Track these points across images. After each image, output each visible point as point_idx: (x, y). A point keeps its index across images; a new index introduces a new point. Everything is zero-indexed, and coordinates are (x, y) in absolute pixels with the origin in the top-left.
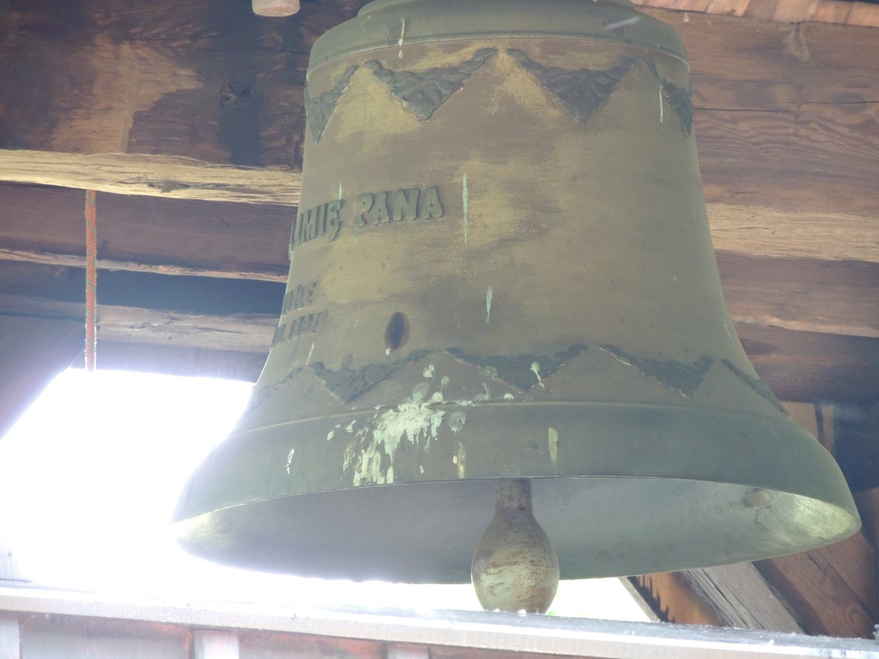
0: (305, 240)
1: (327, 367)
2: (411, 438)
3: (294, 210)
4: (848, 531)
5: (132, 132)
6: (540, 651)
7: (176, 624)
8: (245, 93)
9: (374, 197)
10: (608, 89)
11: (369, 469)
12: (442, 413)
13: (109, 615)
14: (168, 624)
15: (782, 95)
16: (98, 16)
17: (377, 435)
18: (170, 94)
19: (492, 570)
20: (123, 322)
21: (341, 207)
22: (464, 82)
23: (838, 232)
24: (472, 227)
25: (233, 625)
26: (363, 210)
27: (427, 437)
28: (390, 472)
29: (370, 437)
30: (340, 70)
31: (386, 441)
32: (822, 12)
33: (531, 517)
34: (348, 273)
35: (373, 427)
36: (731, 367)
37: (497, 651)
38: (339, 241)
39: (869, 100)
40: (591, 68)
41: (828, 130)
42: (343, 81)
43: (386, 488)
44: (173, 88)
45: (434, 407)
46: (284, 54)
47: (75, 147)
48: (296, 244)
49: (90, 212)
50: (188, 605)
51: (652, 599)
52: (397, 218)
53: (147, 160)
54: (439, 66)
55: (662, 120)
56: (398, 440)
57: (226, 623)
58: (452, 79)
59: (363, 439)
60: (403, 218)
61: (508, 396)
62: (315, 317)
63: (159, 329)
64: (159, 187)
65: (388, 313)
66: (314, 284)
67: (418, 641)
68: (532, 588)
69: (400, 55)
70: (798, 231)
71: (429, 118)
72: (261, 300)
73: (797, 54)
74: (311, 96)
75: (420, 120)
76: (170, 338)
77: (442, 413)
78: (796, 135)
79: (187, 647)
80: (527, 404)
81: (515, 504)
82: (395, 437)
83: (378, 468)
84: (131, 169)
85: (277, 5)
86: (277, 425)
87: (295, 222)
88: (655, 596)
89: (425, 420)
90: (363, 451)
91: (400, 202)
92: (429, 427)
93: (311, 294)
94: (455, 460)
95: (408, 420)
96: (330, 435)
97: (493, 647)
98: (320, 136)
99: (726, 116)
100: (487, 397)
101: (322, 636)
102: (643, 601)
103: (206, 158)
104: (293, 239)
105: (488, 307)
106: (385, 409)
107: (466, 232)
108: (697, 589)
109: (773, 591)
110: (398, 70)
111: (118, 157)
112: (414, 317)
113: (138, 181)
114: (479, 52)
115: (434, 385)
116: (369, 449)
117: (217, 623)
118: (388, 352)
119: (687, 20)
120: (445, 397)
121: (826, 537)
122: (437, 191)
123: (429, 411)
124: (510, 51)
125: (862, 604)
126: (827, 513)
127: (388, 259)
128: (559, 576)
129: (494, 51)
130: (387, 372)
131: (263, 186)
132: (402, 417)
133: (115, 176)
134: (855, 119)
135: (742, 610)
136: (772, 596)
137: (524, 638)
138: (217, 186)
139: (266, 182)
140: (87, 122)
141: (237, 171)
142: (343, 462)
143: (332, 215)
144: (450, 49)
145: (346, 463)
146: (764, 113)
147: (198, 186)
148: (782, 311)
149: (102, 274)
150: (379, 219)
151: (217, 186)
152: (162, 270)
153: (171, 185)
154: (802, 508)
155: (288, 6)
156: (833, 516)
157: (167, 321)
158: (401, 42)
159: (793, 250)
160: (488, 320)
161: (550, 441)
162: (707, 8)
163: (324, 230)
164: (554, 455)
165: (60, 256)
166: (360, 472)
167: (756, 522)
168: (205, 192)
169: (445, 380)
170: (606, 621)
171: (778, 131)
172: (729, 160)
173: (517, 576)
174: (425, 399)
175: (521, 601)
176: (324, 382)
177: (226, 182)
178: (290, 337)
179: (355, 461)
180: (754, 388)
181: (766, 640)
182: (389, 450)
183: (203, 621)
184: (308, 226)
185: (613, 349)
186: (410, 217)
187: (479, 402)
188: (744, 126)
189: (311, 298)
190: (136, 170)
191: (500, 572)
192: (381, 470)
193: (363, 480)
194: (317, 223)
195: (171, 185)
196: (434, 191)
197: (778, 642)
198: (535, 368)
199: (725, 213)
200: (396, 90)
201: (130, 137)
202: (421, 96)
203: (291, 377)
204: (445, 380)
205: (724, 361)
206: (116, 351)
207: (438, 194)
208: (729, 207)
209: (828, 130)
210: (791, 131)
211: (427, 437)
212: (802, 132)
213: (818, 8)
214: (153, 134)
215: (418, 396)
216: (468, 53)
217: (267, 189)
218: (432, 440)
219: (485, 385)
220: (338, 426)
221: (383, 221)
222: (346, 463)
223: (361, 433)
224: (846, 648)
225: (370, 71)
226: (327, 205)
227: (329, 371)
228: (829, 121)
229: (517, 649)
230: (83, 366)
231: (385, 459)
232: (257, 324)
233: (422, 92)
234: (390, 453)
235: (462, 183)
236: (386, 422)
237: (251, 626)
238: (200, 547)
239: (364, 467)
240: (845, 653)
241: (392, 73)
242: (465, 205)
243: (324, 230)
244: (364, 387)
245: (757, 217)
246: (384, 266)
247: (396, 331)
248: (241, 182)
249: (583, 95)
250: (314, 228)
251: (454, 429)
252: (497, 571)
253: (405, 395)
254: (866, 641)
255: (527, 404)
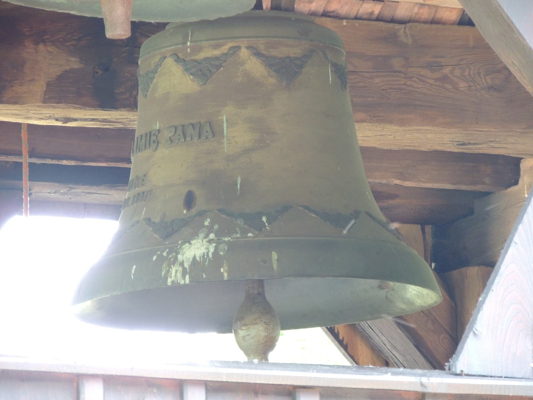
0: (139, 151)
1: (153, 220)
2: (198, 259)
3: (133, 131)
4: (436, 302)
5: (46, 93)
6: (265, 383)
7: (69, 373)
8: (106, 69)
9: (176, 128)
10: (301, 67)
11: (176, 276)
12: (214, 245)
13: (33, 369)
14: (65, 373)
15: (397, 63)
16: (25, 30)
17: (180, 257)
18: (66, 71)
19: (244, 328)
20: (44, 190)
21: (159, 133)
22: (223, 65)
23: (429, 136)
24: (229, 143)
25: (100, 373)
26: (170, 135)
27: (207, 258)
28: (187, 277)
29: (176, 258)
30: (157, 59)
31: (185, 261)
32: (421, 11)
33: (264, 298)
34: (163, 167)
35: (177, 253)
36: (370, 216)
37: (242, 383)
38: (158, 152)
39: (445, 64)
40: (292, 55)
41: (423, 81)
42: (159, 65)
43: (185, 285)
44: (67, 68)
45: (210, 241)
46: (127, 48)
47: (15, 101)
48: (135, 153)
49: (24, 134)
50: (75, 363)
51: (335, 333)
52: (188, 139)
53: (54, 107)
54: (209, 56)
55: (330, 83)
56: (191, 260)
57: (96, 372)
58: (216, 63)
59: (172, 260)
60: (192, 139)
61: (250, 235)
62: (145, 193)
63: (65, 194)
64: (61, 121)
65: (184, 191)
66: (145, 175)
67: (199, 379)
68: (266, 337)
69: (189, 50)
70: (408, 136)
71: (205, 84)
72: (118, 177)
73: (405, 40)
74: (141, 73)
75: (200, 86)
76: (70, 198)
77: (214, 245)
78: (405, 84)
79: (75, 385)
80: (261, 239)
81: (256, 292)
82: (189, 258)
83: (181, 275)
84: (46, 112)
85: (119, 33)
86: (126, 252)
87: (134, 141)
88: (336, 331)
89: (206, 248)
90: (172, 266)
91: (190, 131)
92: (208, 253)
93: (143, 180)
94: (222, 270)
95: (196, 249)
96: (155, 258)
97: (240, 381)
98: (146, 95)
99: (367, 75)
100: (238, 235)
101: (148, 378)
102: (330, 334)
103: (85, 105)
104: (133, 151)
105: (239, 186)
106: (184, 243)
107: (226, 145)
108: (359, 327)
109: (400, 328)
110: (188, 59)
111: (38, 106)
112: (198, 193)
113: (50, 118)
114: (231, 48)
115: (210, 229)
116: (176, 265)
117: (91, 372)
118: (185, 212)
119: (345, 24)
120: (216, 235)
121: (424, 305)
122: (210, 123)
123: (207, 244)
124: (248, 48)
125: (448, 333)
126: (424, 293)
127: (184, 161)
128: (280, 328)
129: (239, 47)
130: (185, 222)
131: (118, 119)
132: (193, 247)
133: (37, 116)
134: (437, 75)
135: (383, 338)
136: (399, 331)
137: (256, 375)
138: (93, 120)
139: (119, 117)
140: (21, 87)
141: (103, 112)
142: (162, 272)
143: (153, 138)
144: (217, 47)
145: (163, 273)
146: (387, 73)
147: (82, 120)
148: (402, 176)
149: (31, 165)
150: (179, 140)
151: (93, 120)
152: (65, 162)
153: (67, 120)
154: (410, 290)
155: (124, 33)
156: (427, 294)
157: (68, 189)
158: (189, 44)
159: (405, 146)
160: (238, 193)
161: (273, 259)
162: (359, 11)
163: (150, 146)
164: (275, 266)
165: (9, 157)
166: (171, 277)
167: (386, 297)
168: (86, 123)
169: (216, 227)
170: (300, 364)
171: (395, 83)
172: (369, 99)
173: (256, 331)
174: (206, 237)
175: (260, 344)
176: (151, 229)
177: (97, 118)
178: (132, 204)
179: (168, 272)
180: (383, 227)
181: (386, 373)
182: (186, 265)
183: (83, 371)
184: (141, 144)
185: (306, 207)
186: (196, 139)
187: (234, 238)
188: (377, 80)
189: (143, 183)
190: (49, 112)
191: (248, 328)
192: (182, 276)
193: (173, 282)
194: (146, 141)
195: (67, 120)
196: (208, 124)
197: (394, 374)
198: (264, 219)
199: (368, 128)
200: (186, 70)
201: (45, 95)
202: (200, 73)
203: (133, 226)
204: (216, 227)
205: (366, 213)
206: (41, 205)
207: (210, 125)
208: (370, 124)
209: (423, 81)
210: (403, 82)
211: (207, 258)
212: (409, 83)
213: (419, 9)
214: (59, 92)
215: (201, 235)
216: (225, 49)
217: (120, 120)
218: (210, 260)
219: (237, 229)
220: (159, 253)
221: (181, 141)
222: (163, 273)
223: (171, 256)
224: (429, 377)
225: (173, 60)
226: (150, 132)
227: (154, 223)
228: (423, 76)
229: (253, 382)
230: (22, 214)
231: (184, 269)
232: (117, 190)
233: (201, 70)
234: (187, 267)
235: (223, 119)
236: (184, 250)
237: (109, 373)
238: (86, 317)
239: (173, 275)
240: (429, 379)
241: (184, 60)
242: (225, 131)
243: (150, 146)
244: (172, 232)
245: (385, 130)
246: (182, 165)
247: (189, 200)
248: (105, 117)
249: (287, 70)
250: (144, 144)
251: (221, 253)
252: (246, 328)
253: (194, 235)
254: (440, 371)
255: (261, 239)
